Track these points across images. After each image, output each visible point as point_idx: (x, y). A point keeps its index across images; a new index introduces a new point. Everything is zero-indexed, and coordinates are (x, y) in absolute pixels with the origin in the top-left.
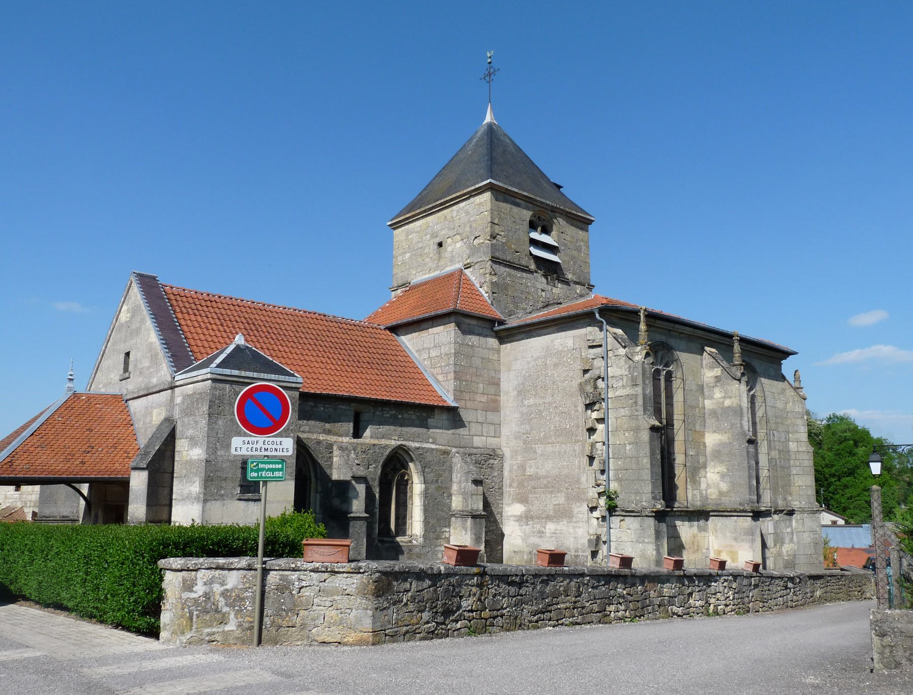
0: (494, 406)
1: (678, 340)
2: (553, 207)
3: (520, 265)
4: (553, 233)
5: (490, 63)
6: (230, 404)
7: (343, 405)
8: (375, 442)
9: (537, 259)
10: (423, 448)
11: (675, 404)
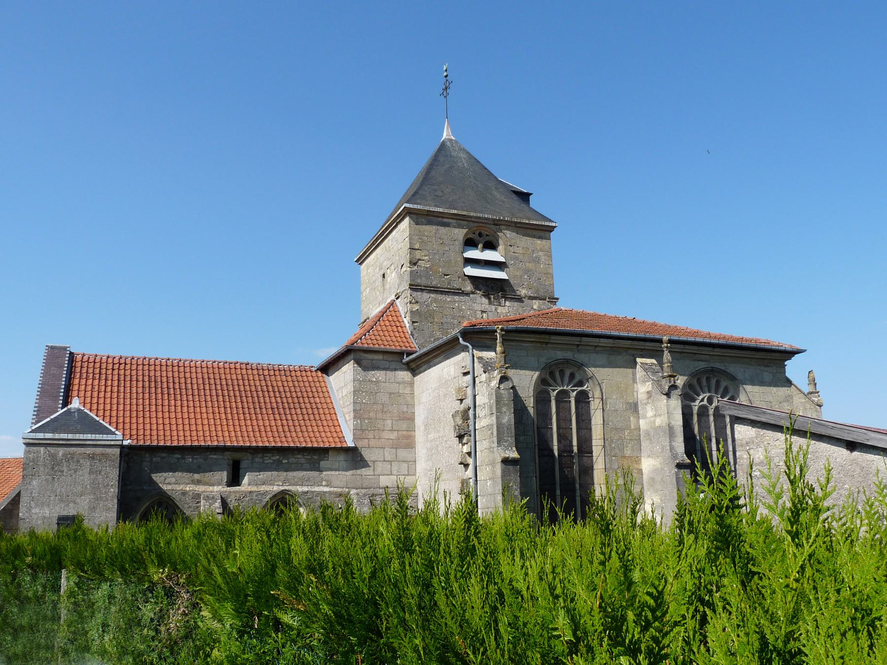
0: (408, 443)
1: (594, 355)
2: (494, 220)
3: (454, 289)
4: (501, 248)
5: (446, 76)
6: (45, 465)
7: (214, 455)
8: (252, 490)
9: (474, 279)
10: (313, 492)
11: (593, 427)
